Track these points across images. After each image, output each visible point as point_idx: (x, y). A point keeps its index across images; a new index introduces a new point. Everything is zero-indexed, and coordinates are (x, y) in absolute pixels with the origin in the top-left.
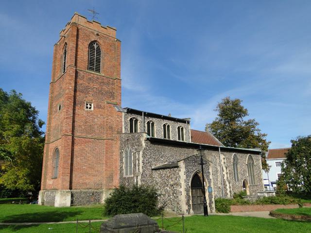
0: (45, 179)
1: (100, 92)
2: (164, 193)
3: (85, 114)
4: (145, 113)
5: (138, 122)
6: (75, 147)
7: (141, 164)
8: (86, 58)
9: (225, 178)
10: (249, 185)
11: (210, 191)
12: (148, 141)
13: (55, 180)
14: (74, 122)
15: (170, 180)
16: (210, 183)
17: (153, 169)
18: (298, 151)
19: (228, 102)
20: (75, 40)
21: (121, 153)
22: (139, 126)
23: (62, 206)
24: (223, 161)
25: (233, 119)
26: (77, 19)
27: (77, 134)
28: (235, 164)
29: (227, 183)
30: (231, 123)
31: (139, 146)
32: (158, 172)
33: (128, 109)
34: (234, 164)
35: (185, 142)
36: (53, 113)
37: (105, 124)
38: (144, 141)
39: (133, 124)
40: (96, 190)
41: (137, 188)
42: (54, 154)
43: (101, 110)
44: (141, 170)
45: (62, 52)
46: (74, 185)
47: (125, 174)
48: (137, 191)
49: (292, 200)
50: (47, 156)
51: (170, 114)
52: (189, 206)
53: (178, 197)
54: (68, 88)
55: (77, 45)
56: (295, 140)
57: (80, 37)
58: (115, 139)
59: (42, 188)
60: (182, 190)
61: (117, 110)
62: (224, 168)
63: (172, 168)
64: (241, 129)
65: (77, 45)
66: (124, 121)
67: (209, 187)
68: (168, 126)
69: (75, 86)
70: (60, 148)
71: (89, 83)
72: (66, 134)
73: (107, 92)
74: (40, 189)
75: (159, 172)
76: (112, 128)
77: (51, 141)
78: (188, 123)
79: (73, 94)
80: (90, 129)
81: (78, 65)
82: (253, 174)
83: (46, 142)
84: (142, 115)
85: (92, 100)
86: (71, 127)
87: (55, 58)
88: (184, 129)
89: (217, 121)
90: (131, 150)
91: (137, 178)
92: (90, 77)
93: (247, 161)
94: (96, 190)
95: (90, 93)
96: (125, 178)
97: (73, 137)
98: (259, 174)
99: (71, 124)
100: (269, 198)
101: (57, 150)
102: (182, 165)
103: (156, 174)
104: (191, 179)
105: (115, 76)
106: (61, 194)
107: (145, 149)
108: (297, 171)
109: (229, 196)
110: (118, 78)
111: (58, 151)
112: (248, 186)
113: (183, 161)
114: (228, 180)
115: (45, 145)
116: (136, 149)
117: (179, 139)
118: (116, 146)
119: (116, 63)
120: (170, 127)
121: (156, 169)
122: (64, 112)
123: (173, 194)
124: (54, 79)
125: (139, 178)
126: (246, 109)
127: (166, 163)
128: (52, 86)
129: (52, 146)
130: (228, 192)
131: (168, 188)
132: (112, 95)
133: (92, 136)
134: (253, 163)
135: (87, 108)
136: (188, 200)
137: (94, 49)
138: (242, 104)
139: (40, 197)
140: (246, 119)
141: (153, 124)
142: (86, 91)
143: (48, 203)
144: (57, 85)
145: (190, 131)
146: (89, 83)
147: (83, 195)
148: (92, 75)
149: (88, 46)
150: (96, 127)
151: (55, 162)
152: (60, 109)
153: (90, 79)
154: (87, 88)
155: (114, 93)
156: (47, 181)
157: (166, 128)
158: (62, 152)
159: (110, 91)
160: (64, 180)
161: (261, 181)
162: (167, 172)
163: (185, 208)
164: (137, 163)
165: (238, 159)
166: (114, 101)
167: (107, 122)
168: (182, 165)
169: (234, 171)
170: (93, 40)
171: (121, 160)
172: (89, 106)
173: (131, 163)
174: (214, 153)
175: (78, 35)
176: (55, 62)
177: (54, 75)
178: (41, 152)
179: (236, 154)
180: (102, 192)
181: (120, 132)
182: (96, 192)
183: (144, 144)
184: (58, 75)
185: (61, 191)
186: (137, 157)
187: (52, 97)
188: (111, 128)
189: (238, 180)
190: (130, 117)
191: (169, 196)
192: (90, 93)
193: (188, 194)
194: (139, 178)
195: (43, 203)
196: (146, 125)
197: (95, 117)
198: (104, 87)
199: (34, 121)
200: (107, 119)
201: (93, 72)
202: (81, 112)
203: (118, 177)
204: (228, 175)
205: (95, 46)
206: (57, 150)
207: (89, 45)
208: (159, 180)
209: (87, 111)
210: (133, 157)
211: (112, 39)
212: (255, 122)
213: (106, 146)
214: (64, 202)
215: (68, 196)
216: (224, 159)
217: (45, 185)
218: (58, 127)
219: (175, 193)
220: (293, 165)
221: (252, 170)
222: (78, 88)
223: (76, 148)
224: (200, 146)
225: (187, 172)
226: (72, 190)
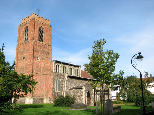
3: (37, 63)
4: (62, 63)
12: (68, 77)
15: (78, 94)
16: (93, 95)
17: (69, 89)
18: (126, 82)
21: (53, 81)
23: (29, 103)
31: (64, 79)
33: (56, 61)
39: (57, 67)
40: (41, 98)
44: (65, 89)
47: (55, 91)
49: (123, 102)
56: (126, 77)
58: (50, 75)
60: (84, 97)
66: (54, 65)
68: (72, 69)
72: (30, 71)
80: (39, 70)
84: (61, 64)
90: (59, 80)
94: (41, 98)
99: (32, 67)
102: (84, 87)
103: (71, 91)
108: (125, 91)
110: (51, 45)
116: (62, 80)
117: (76, 75)
123: (79, 99)
125: (65, 92)
127: (74, 87)
128: (18, 47)
131: (77, 97)
135: (38, 59)
136: (86, 102)
137: (41, 31)
141: (65, 68)
142: (37, 52)
144: (21, 47)
145: (80, 71)
148: (40, 43)
150: (41, 68)
153: (39, 45)
154: (38, 50)
163: (92, 106)
170: (41, 26)
172: (39, 59)
176: (19, 34)
180: (44, 98)
181: (52, 72)
183: (66, 78)
187: (18, 52)
193: (85, 99)
194: (65, 92)
197: (41, 64)
198: (45, 49)
201: (40, 42)
203: (52, 92)
205: (41, 29)
209: (38, 61)
210: (60, 83)
211: (49, 26)
214: (30, 102)
220: (124, 88)
225: (86, 90)
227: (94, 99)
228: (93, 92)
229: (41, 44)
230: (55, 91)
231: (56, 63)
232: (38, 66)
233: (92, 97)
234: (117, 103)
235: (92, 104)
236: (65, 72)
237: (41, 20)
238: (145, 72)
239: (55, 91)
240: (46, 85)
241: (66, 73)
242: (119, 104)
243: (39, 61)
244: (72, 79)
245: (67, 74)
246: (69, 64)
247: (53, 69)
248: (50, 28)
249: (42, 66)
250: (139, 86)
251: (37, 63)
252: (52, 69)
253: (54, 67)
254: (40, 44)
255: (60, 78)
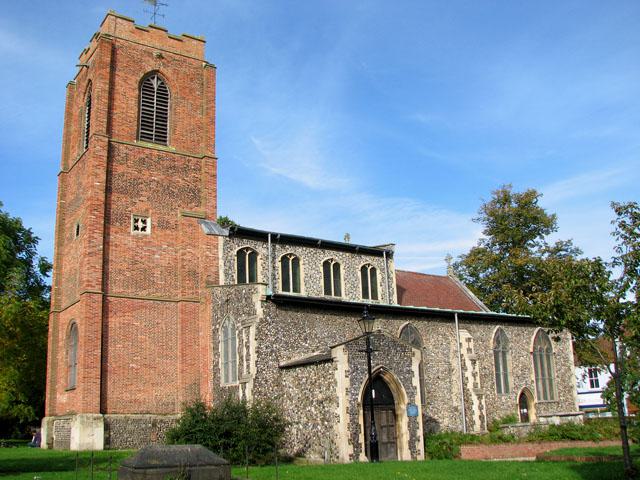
0: (54, 391)
1: (168, 191)
2: (305, 419)
3: (132, 244)
4: (274, 236)
5: (259, 257)
6: (110, 319)
7: (254, 357)
8: (133, 112)
9: (470, 386)
10: (536, 401)
11: (413, 413)
12: (270, 304)
13: (71, 394)
14: (105, 262)
16: (412, 395)
17: (282, 368)
19: (506, 200)
20: (108, 76)
21: (215, 331)
22: (259, 269)
23: (84, 448)
24: (465, 345)
25: (520, 243)
26: (113, 26)
27: (114, 289)
28: (500, 354)
29: (474, 398)
30: (513, 252)
31: (249, 314)
32: (292, 373)
34: (496, 353)
35: (381, 304)
36: (66, 242)
37: (179, 266)
38: (260, 303)
39: (245, 267)
40: (160, 417)
41: (191, 410)
42: (68, 337)
43: (168, 232)
44: (253, 370)
45: (81, 102)
46: (110, 404)
48: (234, 411)
50: (56, 341)
51: (347, 236)
52: (357, 446)
53: (331, 427)
54: (92, 186)
55: (112, 84)
57: (119, 66)
59: (47, 410)
60: (341, 410)
61: (206, 230)
62: (468, 363)
63: (320, 362)
64: (539, 263)
65: (112, 84)
66: (223, 256)
67: (411, 404)
69: (108, 181)
70: (78, 321)
71: (140, 172)
72: (90, 289)
73: (182, 190)
74: (43, 415)
75: (295, 374)
76: (195, 273)
77: (63, 306)
78: (389, 255)
79: (103, 199)
80: (144, 278)
81: (116, 130)
82: (550, 375)
83: (52, 309)
84: (382, 256)
85: (147, 210)
86: (99, 275)
87: (69, 114)
88: (378, 272)
89: (482, 246)
91: (244, 389)
92: (142, 156)
93: (532, 345)
95: (144, 193)
96: (223, 389)
97: (105, 297)
98: (563, 375)
99: (99, 266)
100: (559, 427)
101: (73, 326)
102: (340, 355)
103: (288, 379)
104: (362, 386)
105: (202, 150)
106: (82, 423)
107: (262, 321)
109: (477, 428)
111: (76, 329)
112: (532, 404)
113: (343, 346)
114: (474, 390)
115: (52, 317)
116: (243, 323)
117: (365, 295)
118: (207, 313)
119: (204, 120)
120: (342, 267)
121: (288, 367)
122: (85, 239)
123: (323, 420)
124: (65, 164)
126: (554, 216)
128: (63, 181)
129: (65, 318)
130: (476, 418)
131: (313, 409)
132: (194, 195)
133: (149, 294)
134: (549, 349)
135: (136, 228)
137: (153, 93)
138: (541, 203)
139: (44, 432)
140: (551, 240)
141: (296, 261)
142: (133, 189)
143: (60, 443)
144: (72, 179)
145: (393, 276)
146: (140, 172)
147: (130, 427)
148: (147, 152)
149: (136, 86)
150: (157, 273)
151: (71, 353)
152: (78, 234)
153: (142, 161)
155: (199, 191)
156: (58, 397)
157: (331, 272)
158: (81, 330)
159: (192, 182)
160: (87, 391)
161: (569, 391)
162: (309, 373)
163: (345, 450)
164: (245, 353)
165: (507, 340)
166: (201, 210)
167: (183, 259)
168: (340, 355)
169: (497, 369)
170: (149, 69)
171: (216, 348)
173: (234, 355)
174: (442, 327)
175: (113, 62)
176: (67, 125)
177: (66, 155)
178: (44, 330)
179: (503, 327)
182: (161, 421)
183: (260, 311)
184: (75, 154)
185: (82, 417)
186: (245, 340)
188: (193, 274)
189: (507, 391)
190: (237, 246)
191: (314, 426)
192: (144, 193)
193: (353, 422)
195: (50, 445)
196: (279, 265)
198: (176, 178)
199: (28, 263)
200: (184, 254)
201: (150, 145)
202: (124, 239)
203: (210, 386)
204: (478, 378)
205: (155, 83)
206: (73, 326)
207: (141, 82)
208: (294, 391)
212: (573, 248)
213: (180, 315)
214: (88, 440)
215: (98, 427)
216: (469, 340)
217: (53, 407)
218: (75, 274)
219: (327, 419)
221: (546, 366)
222: (116, 183)
223: (114, 322)
224: (421, 308)
225: (352, 374)
226: (106, 416)
227: (416, 415)
228: (408, 381)
229: (156, 153)
230: (223, 384)
231: (236, 240)
232: (135, 263)
233: (403, 407)
234: (573, 439)
235: (406, 446)
236: (253, 279)
237: (151, 41)
238: (613, 204)
239: (223, 384)
240: (183, 355)
241: (260, 281)
242: (590, 444)
243: (146, 236)
244: (299, 315)
245: (261, 288)
246: (317, 241)
247: (217, 273)
248: (204, 77)
249: (162, 259)
250: (170, 297)
251: (132, 244)
252: (213, 270)
253: (226, 260)
254: (149, 157)
255: (237, 314)
